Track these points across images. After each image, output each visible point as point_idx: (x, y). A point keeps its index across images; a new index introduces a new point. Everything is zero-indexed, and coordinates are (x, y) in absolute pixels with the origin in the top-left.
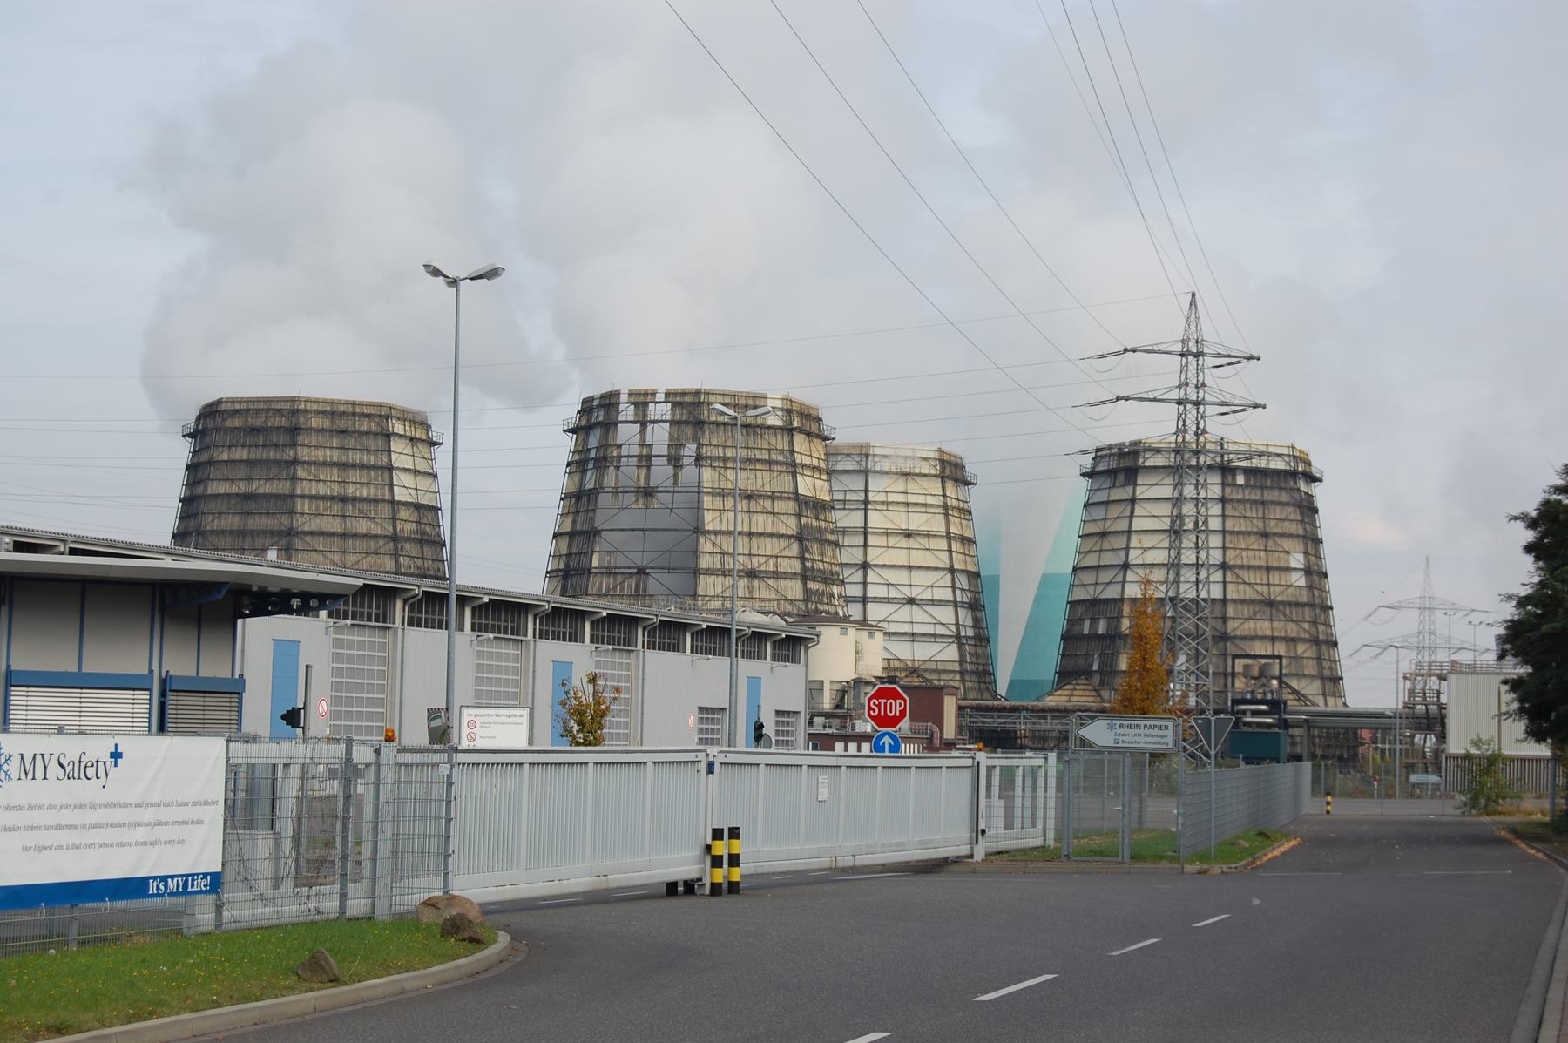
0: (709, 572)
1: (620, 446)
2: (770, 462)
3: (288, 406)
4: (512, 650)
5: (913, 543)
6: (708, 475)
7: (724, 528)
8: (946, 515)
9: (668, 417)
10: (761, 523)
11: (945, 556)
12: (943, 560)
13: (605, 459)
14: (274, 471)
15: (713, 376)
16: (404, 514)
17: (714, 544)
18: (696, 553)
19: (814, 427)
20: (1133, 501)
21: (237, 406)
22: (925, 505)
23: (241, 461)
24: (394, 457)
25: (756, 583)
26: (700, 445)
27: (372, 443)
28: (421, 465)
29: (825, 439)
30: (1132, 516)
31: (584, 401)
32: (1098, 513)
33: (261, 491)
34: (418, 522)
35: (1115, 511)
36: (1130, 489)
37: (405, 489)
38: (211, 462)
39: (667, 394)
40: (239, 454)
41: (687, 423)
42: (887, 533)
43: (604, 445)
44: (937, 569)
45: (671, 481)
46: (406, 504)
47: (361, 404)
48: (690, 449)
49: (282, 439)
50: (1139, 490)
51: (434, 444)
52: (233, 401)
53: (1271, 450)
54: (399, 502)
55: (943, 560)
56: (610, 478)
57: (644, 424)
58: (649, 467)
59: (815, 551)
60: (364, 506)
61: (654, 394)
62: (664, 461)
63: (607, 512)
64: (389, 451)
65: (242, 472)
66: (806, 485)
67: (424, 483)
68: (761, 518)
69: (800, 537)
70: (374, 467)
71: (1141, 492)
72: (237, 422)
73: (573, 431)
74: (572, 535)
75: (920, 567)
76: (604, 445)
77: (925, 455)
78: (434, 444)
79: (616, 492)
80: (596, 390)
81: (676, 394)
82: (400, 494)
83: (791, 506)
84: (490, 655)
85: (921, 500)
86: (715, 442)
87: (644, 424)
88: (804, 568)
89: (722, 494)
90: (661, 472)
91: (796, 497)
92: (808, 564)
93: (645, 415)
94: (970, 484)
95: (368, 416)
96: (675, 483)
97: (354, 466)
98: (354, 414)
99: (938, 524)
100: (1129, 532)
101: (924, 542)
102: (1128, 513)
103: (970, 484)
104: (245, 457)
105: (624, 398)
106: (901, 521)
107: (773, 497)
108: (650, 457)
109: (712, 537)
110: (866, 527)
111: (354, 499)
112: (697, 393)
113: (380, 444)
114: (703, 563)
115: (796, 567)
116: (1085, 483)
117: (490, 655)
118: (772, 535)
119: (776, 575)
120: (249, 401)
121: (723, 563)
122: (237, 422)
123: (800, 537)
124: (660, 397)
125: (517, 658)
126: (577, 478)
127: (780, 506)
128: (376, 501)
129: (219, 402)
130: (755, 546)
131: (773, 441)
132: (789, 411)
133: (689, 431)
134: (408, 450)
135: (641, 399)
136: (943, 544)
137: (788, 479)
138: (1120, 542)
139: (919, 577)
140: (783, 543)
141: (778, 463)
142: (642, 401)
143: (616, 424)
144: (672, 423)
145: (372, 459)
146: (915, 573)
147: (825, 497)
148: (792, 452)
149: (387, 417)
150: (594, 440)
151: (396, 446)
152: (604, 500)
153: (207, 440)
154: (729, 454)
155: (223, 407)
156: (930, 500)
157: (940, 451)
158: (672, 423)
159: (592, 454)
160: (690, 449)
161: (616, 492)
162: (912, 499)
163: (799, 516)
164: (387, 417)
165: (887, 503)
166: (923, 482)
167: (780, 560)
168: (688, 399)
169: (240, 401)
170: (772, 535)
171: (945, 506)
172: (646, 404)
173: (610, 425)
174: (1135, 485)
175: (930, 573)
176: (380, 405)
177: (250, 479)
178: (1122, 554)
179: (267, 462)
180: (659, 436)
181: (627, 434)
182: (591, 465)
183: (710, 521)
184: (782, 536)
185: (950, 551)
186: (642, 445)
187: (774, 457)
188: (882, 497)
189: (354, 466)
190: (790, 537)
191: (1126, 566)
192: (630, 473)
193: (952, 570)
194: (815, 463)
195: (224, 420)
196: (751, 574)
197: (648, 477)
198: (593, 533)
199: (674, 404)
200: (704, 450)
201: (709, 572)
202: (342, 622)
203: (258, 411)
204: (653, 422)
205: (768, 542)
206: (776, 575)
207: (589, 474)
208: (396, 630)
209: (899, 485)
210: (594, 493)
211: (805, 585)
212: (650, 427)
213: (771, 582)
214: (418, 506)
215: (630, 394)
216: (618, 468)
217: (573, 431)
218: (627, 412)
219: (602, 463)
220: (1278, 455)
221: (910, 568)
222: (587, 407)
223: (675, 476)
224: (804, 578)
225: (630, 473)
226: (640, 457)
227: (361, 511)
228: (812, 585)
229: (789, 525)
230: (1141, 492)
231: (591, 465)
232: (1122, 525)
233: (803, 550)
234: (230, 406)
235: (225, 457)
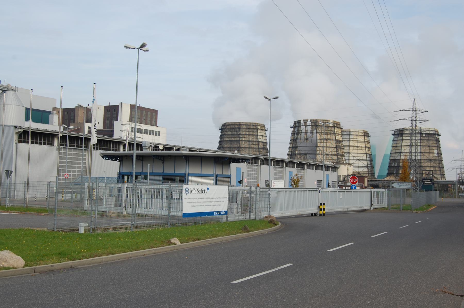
0: (319, 154)
2: (330, 133)
5: (358, 148)
10: (329, 145)
14: (236, 136)
16: (260, 144)
18: (316, 151)
19: (339, 126)
20: (402, 140)
28: (264, 135)
35: (399, 142)
37: (260, 139)
38: (224, 134)
48: (315, 131)
49: (238, 130)
56: (299, 137)
57: (306, 126)
59: (339, 150)
63: (299, 143)
65: (230, 136)
66: (337, 138)
67: (264, 138)
69: (336, 147)
71: (404, 138)
72: (229, 127)
74: (292, 147)
76: (298, 130)
79: (301, 139)
83: (334, 142)
84: (277, 170)
87: (306, 126)
89: (321, 139)
90: (309, 135)
99: (363, 145)
100: (402, 146)
101: (361, 148)
105: (302, 121)
106: (356, 144)
107: (331, 140)
108: (307, 132)
112: (316, 120)
113: (256, 130)
114: (318, 152)
115: (336, 153)
116: (393, 136)
117: (277, 170)
119: (332, 155)
120: (231, 123)
123: (336, 148)
124: (309, 121)
127: (332, 141)
133: (314, 127)
136: (365, 149)
137: (334, 136)
138: (400, 148)
140: (333, 149)
142: (305, 122)
143: (300, 126)
150: (296, 129)
151: (259, 131)
152: (298, 141)
160: (315, 131)
161: (301, 139)
163: (336, 143)
166: (360, 136)
171: (365, 141)
173: (299, 126)
177: (232, 138)
180: (309, 128)
181: (302, 128)
183: (319, 145)
188: (352, 140)
192: (303, 136)
196: (327, 155)
198: (296, 147)
199: (312, 122)
201: (319, 154)
206: (332, 155)
209: (356, 137)
210: (296, 139)
214: (263, 142)
218: (303, 124)
219: (298, 134)
222: (295, 123)
224: (337, 155)
225: (303, 136)
229: (334, 145)
230: (404, 138)
232: (400, 145)
233: (337, 150)
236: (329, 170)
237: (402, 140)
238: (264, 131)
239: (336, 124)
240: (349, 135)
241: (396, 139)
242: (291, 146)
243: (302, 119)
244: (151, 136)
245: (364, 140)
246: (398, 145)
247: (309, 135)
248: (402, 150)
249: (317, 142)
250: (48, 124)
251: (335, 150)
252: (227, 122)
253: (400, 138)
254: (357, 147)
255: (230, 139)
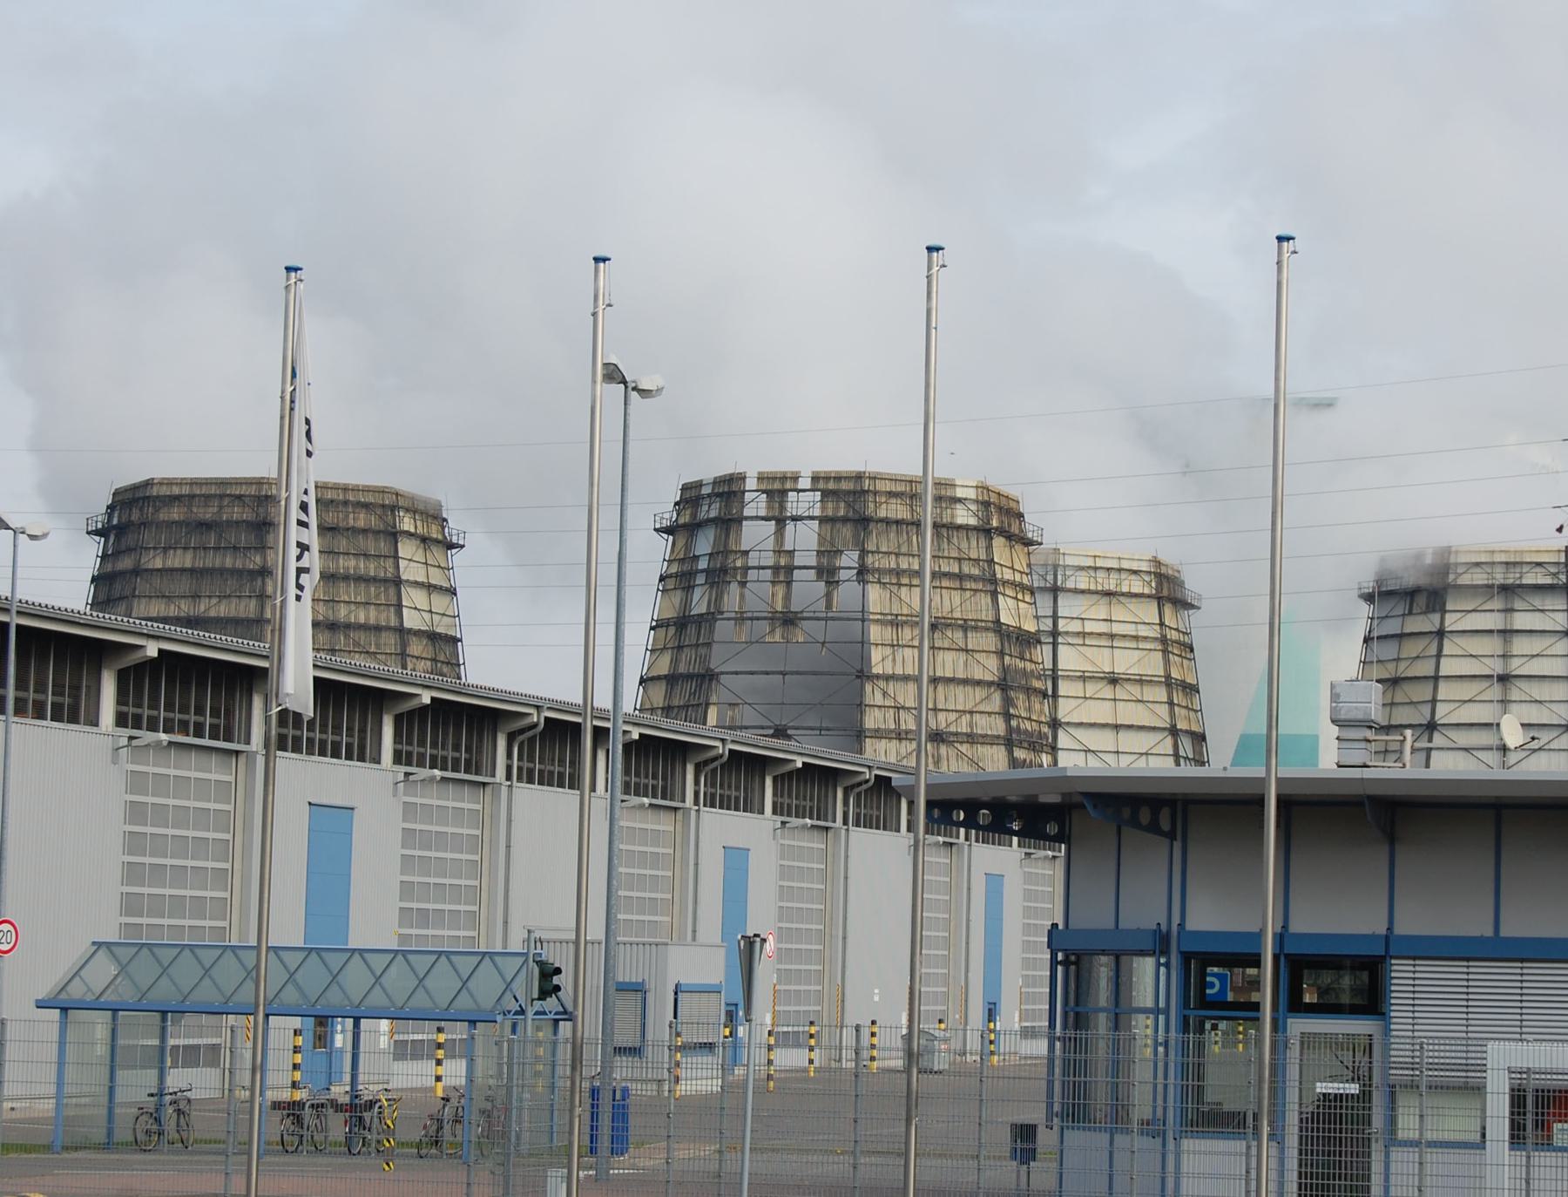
0: (879, 734)
1: (746, 553)
2: (960, 577)
3: (253, 490)
4: (466, 802)
5: (1121, 692)
6: (876, 597)
7: (899, 671)
8: (1165, 652)
9: (817, 513)
10: (949, 664)
11: (1163, 710)
12: (1161, 716)
13: (724, 570)
14: (232, 583)
15: (885, 452)
16: (416, 647)
17: (885, 694)
18: (861, 706)
19: (1015, 529)
20: (1441, 634)
21: (176, 491)
22: (1136, 638)
23: (183, 570)
24: (402, 563)
25: (943, 749)
26: (864, 553)
27: (371, 545)
28: (436, 578)
29: (1028, 543)
30: (1439, 655)
31: (685, 488)
32: (1389, 650)
33: (213, 613)
34: (434, 660)
35: (1412, 648)
36: (1436, 617)
37: (416, 612)
38: (137, 572)
39: (815, 478)
40: (181, 560)
41: (845, 520)
42: (1084, 678)
43: (722, 551)
44: (1154, 729)
45: (822, 603)
46: (418, 633)
47: (356, 489)
48: (850, 559)
49: (244, 539)
50: (1449, 618)
51: (451, 546)
52: (170, 482)
53: (1125, 565)
54: (410, 631)
55: (1161, 716)
56: (732, 598)
57: (781, 522)
58: (789, 583)
59: (1021, 704)
60: (362, 637)
61: (795, 478)
62: (812, 574)
63: (728, 648)
64: (396, 557)
65: (184, 585)
66: (1012, 612)
67: (439, 602)
68: (949, 657)
69: (1003, 685)
70: (375, 580)
71: (1451, 622)
72: (176, 514)
73: (669, 530)
74: (671, 679)
75: (1130, 727)
76: (722, 551)
77: (1135, 566)
78: (451, 546)
79: (741, 618)
80: (708, 470)
81: (827, 479)
82: (411, 620)
83: (990, 641)
84: (428, 812)
85: (1129, 630)
86: (884, 549)
87: (781, 522)
88: (1009, 729)
89: (895, 623)
90: (807, 589)
91: (997, 626)
92: (1014, 723)
93: (782, 508)
94: (1192, 606)
95: (366, 506)
96: (829, 606)
97: (346, 578)
98: (346, 503)
99: (1153, 665)
100: (1436, 678)
101: (1135, 690)
102: (1433, 651)
103: (1192, 606)
104: (188, 564)
105: (751, 484)
106: (1103, 660)
107: (966, 627)
108: (790, 569)
109: (882, 684)
110: (1055, 669)
111: (348, 626)
112: (859, 477)
113: (383, 546)
114: (872, 720)
115: (998, 727)
116: (1365, 609)
117: (428, 812)
118: (965, 682)
119: (971, 739)
120: (194, 482)
121: (897, 721)
122: (176, 514)
123: (1003, 685)
124: (804, 483)
125: (476, 819)
126: (677, 598)
127: (976, 640)
128: (378, 629)
129: (148, 484)
130: (941, 697)
131: (964, 545)
132: (986, 504)
133: (847, 531)
134: (419, 556)
135: (777, 486)
136: (1161, 694)
137: (985, 600)
138: (1422, 692)
139: (1130, 741)
140: (980, 693)
141: (971, 577)
142: (778, 488)
143: (740, 520)
144: (823, 520)
145: (371, 568)
146: (1122, 734)
147: (1030, 626)
148: (991, 562)
149: (393, 508)
150: (704, 544)
151: (406, 549)
152: (723, 629)
153: (130, 540)
154: (904, 566)
155: (155, 491)
156: (1144, 631)
157: (1156, 562)
158: (823, 520)
159: (703, 564)
160: (850, 559)
161: (741, 618)
162: (1117, 629)
163: (1001, 654)
164: (393, 508)
165: (1083, 635)
166: (1133, 605)
167: (977, 717)
168: (845, 486)
169: (181, 482)
170: (965, 682)
171: (1164, 640)
172: (784, 493)
173: (729, 523)
174: (1444, 611)
175: (1142, 735)
176: (382, 491)
177: (196, 597)
178: (1426, 710)
179: (222, 571)
180: (804, 539)
181: (755, 536)
182: (700, 579)
183: (879, 661)
184: (979, 683)
185: (1171, 703)
186: (778, 552)
187: (966, 570)
188: (1075, 626)
189: (346, 578)
190: (990, 684)
191: (1431, 727)
192: (760, 593)
193: (1174, 731)
194: (1018, 577)
195: (157, 511)
196: (937, 737)
197: (787, 597)
198: (707, 678)
199: (826, 494)
200: (870, 560)
201: (879, 734)
202: (147, 737)
203: (208, 497)
204: (795, 519)
205: (960, 691)
206: (971, 739)
207: (698, 593)
208: (251, 756)
209: (1101, 610)
210: (709, 618)
211: (1010, 752)
212: (790, 526)
213: (964, 748)
214: (433, 637)
215: (761, 478)
216: (743, 584)
217: (669, 530)
218: (755, 504)
219: (719, 576)
220: (1135, 572)
221: (1117, 727)
222: (691, 496)
223: (828, 596)
224: (1009, 743)
225: (760, 593)
226: (776, 569)
227: (356, 644)
228: (1020, 754)
229: (988, 668)
230: (1451, 622)
231: (700, 579)
232: (1426, 668)
233: (1008, 702)
234: (164, 491)
235: (158, 564)
236: (751, 805)
237: (1441, 634)
238: (437, 554)
239: (1000, 509)
240: (1055, 590)
241: (1392, 627)
242: (664, 667)
243: (752, 463)
244: (116, 858)
245: (1154, 632)
246: (1404, 670)
247: (807, 589)
248: (1441, 710)
249: (864, 643)
250: (1317, 737)
251: (997, 698)
252: (158, 473)
253: (1429, 623)
254: (1113, 680)
255: (185, 608)
